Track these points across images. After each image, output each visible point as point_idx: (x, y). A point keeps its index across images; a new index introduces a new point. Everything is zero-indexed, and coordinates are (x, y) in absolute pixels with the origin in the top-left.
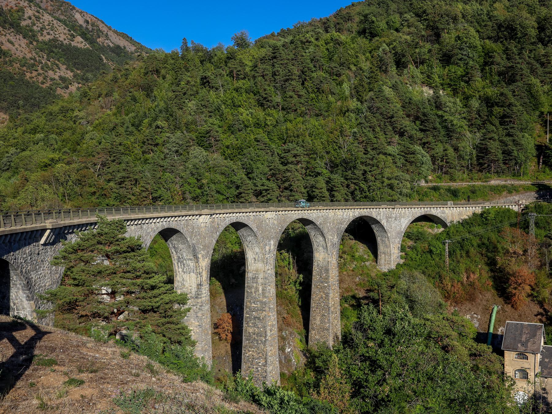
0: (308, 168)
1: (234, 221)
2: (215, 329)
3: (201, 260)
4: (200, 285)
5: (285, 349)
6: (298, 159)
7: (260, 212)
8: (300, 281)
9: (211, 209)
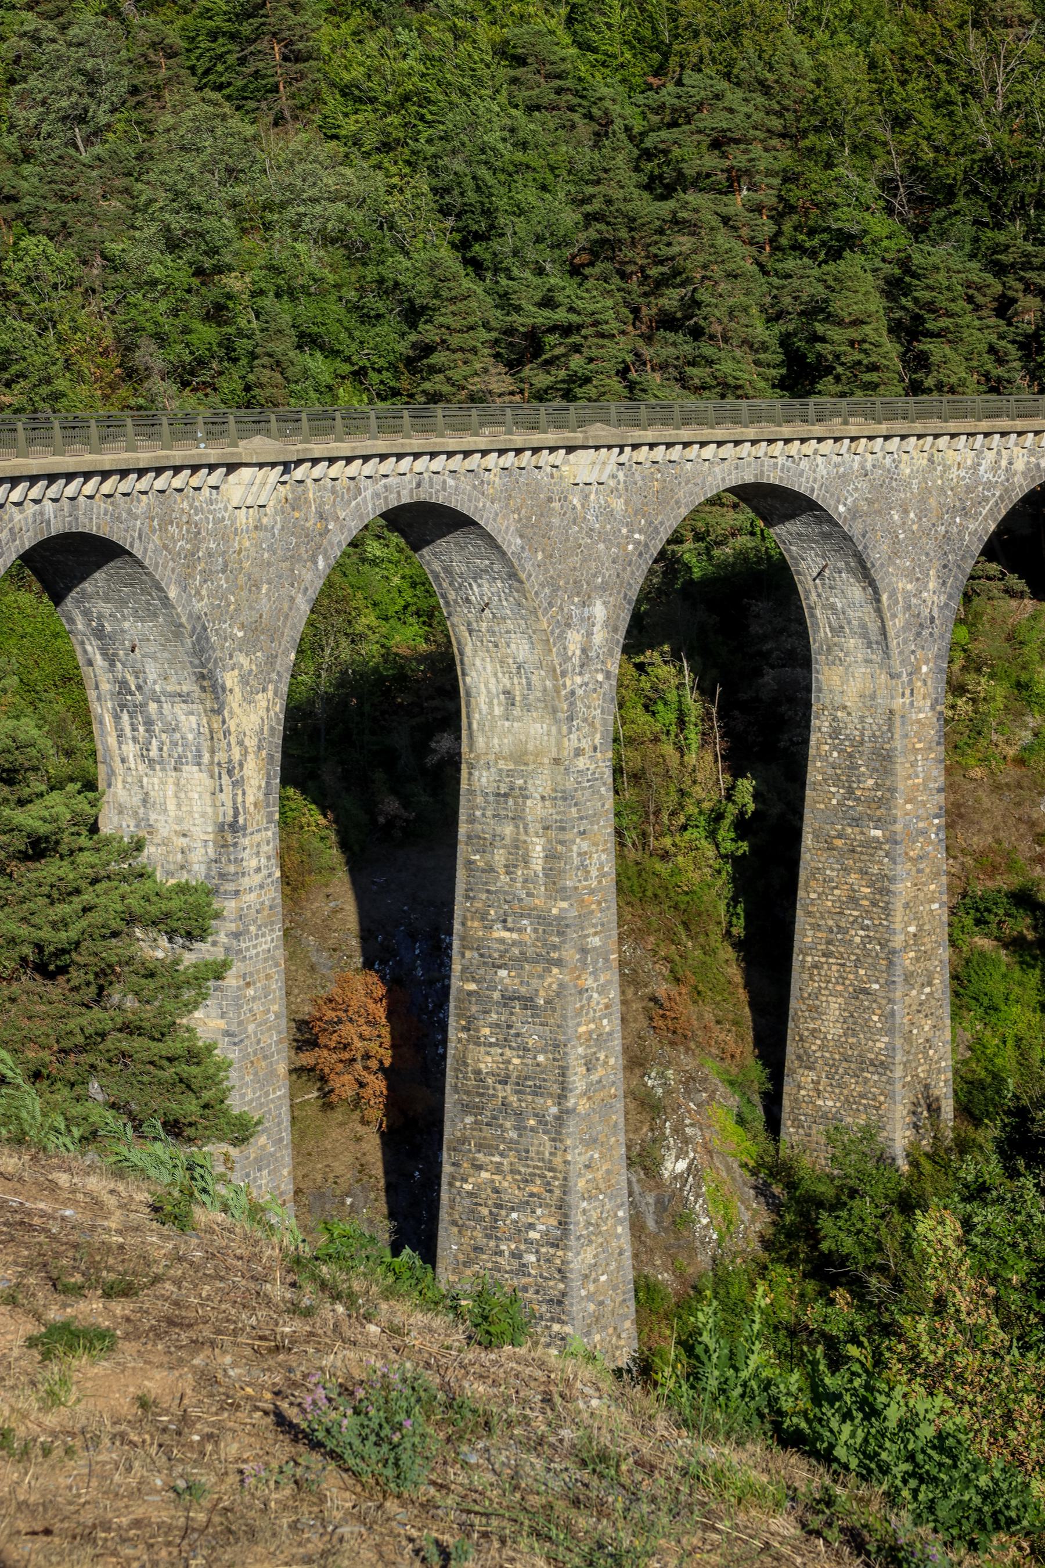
0: (791, 209)
1: (405, 500)
2: (299, 1049)
3: (234, 701)
4: (234, 827)
5: (659, 1163)
6: (737, 157)
7: (536, 450)
8: (742, 813)
9: (282, 435)
